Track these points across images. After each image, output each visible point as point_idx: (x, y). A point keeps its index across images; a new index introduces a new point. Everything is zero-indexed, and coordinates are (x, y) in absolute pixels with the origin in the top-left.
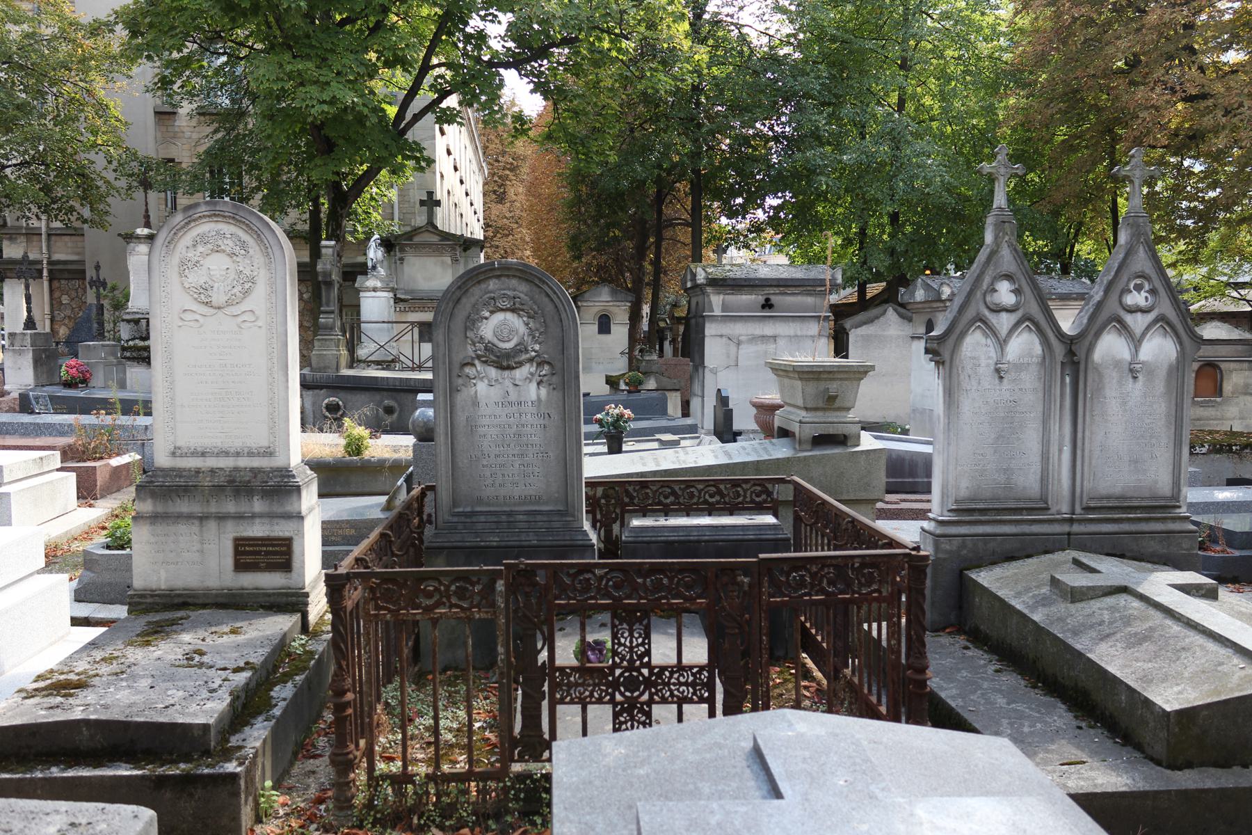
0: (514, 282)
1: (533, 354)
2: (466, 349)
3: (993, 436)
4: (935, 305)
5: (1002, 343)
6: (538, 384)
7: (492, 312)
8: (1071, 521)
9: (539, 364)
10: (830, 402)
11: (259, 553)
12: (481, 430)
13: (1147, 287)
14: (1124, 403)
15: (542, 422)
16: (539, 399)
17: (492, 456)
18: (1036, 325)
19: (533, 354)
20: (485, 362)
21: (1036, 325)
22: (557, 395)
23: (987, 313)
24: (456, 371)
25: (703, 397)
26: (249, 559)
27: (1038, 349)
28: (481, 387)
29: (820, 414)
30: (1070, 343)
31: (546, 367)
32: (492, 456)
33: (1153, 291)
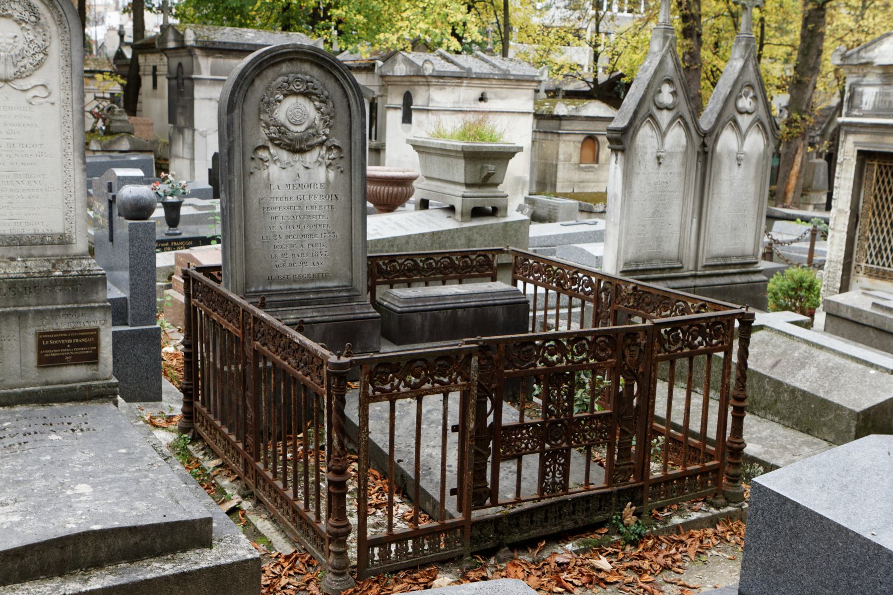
0: (306, 67)
1: (324, 137)
2: (259, 131)
3: (652, 210)
4: (415, 79)
5: (663, 135)
6: (327, 167)
7: (285, 96)
8: (695, 276)
9: (329, 149)
10: (487, 182)
11: (64, 346)
12: (273, 212)
13: (751, 94)
14: (731, 185)
15: (331, 204)
16: (328, 182)
17: (283, 237)
18: (686, 124)
19: (324, 137)
20: (278, 145)
21: (686, 124)
22: (345, 178)
23: (654, 110)
24: (250, 154)
25: (192, 160)
26: (54, 353)
27: (684, 141)
28: (274, 170)
29: (474, 190)
30: (704, 135)
31: (335, 151)
32: (283, 237)
33: (755, 98)
